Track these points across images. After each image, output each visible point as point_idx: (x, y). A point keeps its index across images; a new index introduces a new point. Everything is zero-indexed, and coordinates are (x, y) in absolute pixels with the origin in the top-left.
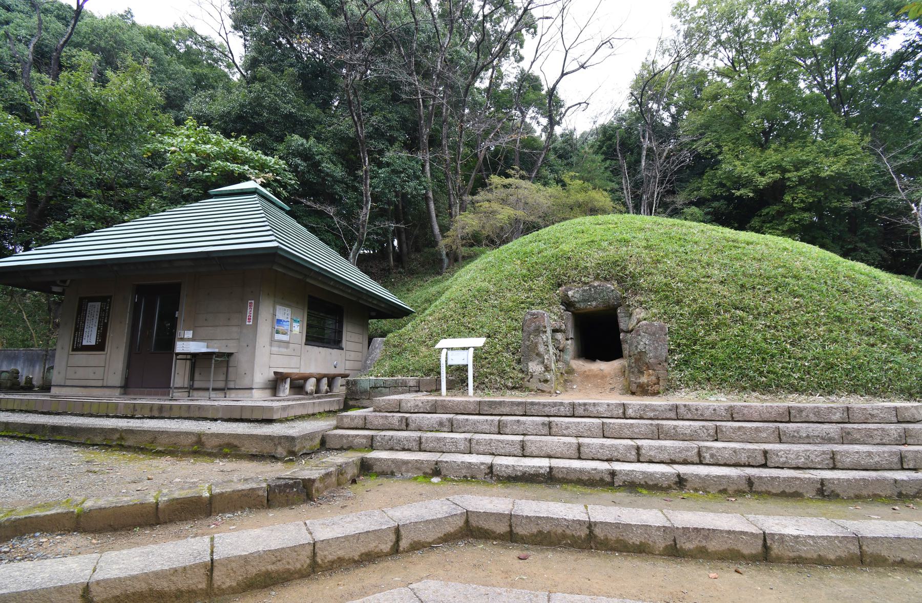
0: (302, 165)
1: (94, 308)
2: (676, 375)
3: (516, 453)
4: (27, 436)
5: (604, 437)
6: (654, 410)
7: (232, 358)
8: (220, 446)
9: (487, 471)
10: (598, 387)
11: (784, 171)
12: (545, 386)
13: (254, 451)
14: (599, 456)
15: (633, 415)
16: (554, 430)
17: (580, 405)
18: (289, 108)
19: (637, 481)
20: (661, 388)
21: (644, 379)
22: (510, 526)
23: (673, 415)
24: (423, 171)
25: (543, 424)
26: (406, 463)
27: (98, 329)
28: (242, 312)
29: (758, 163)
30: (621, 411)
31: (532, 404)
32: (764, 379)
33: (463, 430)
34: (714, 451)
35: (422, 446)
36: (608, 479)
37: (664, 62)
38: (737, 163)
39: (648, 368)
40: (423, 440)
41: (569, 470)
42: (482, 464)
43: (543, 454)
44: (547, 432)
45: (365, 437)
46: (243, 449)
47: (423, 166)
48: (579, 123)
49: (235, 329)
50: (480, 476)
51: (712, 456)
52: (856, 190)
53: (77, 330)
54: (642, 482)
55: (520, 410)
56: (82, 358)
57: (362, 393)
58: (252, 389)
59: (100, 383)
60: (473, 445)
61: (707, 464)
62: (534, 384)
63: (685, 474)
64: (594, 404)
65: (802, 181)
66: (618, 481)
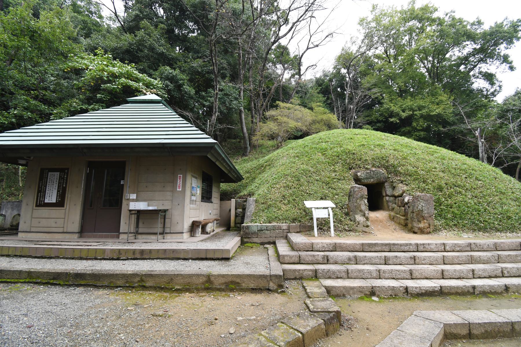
0: (171, 86)
1: (54, 178)
2: (437, 223)
3: (407, 277)
4: (52, 281)
5: (444, 264)
6: (459, 247)
7: (167, 213)
8: (225, 283)
9: (404, 291)
10: (381, 229)
11: (414, 111)
12: (366, 229)
13: (252, 286)
14: (454, 276)
15: (449, 250)
16: (417, 261)
17: (421, 244)
18: (161, 49)
19: (486, 290)
20: (432, 230)
21: (421, 225)
22: (470, 330)
23: (469, 249)
24: (239, 96)
25: (411, 258)
26: (352, 288)
27: (58, 191)
28: (174, 182)
29: (402, 105)
30: (443, 248)
31: (394, 244)
32: (482, 225)
33: (363, 262)
34: (509, 270)
35: (349, 276)
36: (471, 290)
37: (354, 49)
38: (392, 105)
39: (424, 219)
40: (350, 271)
41: (451, 288)
42: (401, 287)
43: (423, 277)
44: (413, 263)
45: (311, 270)
46: (243, 285)
47: (240, 92)
48: (309, 76)
49: (169, 193)
50: (401, 295)
51: (508, 272)
52: (445, 123)
53: (39, 191)
54: (489, 291)
55: (387, 249)
56: (44, 212)
57: (252, 234)
58: (183, 233)
59: (61, 230)
60: (381, 274)
61: (506, 277)
62: (360, 228)
63: (509, 285)
64: (429, 244)
65: (422, 116)
66: (477, 292)
